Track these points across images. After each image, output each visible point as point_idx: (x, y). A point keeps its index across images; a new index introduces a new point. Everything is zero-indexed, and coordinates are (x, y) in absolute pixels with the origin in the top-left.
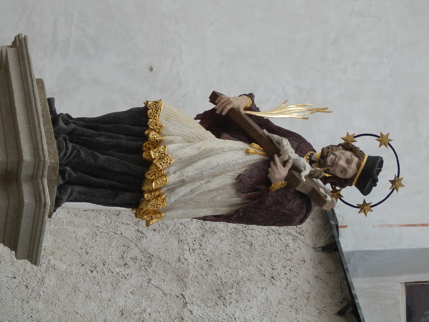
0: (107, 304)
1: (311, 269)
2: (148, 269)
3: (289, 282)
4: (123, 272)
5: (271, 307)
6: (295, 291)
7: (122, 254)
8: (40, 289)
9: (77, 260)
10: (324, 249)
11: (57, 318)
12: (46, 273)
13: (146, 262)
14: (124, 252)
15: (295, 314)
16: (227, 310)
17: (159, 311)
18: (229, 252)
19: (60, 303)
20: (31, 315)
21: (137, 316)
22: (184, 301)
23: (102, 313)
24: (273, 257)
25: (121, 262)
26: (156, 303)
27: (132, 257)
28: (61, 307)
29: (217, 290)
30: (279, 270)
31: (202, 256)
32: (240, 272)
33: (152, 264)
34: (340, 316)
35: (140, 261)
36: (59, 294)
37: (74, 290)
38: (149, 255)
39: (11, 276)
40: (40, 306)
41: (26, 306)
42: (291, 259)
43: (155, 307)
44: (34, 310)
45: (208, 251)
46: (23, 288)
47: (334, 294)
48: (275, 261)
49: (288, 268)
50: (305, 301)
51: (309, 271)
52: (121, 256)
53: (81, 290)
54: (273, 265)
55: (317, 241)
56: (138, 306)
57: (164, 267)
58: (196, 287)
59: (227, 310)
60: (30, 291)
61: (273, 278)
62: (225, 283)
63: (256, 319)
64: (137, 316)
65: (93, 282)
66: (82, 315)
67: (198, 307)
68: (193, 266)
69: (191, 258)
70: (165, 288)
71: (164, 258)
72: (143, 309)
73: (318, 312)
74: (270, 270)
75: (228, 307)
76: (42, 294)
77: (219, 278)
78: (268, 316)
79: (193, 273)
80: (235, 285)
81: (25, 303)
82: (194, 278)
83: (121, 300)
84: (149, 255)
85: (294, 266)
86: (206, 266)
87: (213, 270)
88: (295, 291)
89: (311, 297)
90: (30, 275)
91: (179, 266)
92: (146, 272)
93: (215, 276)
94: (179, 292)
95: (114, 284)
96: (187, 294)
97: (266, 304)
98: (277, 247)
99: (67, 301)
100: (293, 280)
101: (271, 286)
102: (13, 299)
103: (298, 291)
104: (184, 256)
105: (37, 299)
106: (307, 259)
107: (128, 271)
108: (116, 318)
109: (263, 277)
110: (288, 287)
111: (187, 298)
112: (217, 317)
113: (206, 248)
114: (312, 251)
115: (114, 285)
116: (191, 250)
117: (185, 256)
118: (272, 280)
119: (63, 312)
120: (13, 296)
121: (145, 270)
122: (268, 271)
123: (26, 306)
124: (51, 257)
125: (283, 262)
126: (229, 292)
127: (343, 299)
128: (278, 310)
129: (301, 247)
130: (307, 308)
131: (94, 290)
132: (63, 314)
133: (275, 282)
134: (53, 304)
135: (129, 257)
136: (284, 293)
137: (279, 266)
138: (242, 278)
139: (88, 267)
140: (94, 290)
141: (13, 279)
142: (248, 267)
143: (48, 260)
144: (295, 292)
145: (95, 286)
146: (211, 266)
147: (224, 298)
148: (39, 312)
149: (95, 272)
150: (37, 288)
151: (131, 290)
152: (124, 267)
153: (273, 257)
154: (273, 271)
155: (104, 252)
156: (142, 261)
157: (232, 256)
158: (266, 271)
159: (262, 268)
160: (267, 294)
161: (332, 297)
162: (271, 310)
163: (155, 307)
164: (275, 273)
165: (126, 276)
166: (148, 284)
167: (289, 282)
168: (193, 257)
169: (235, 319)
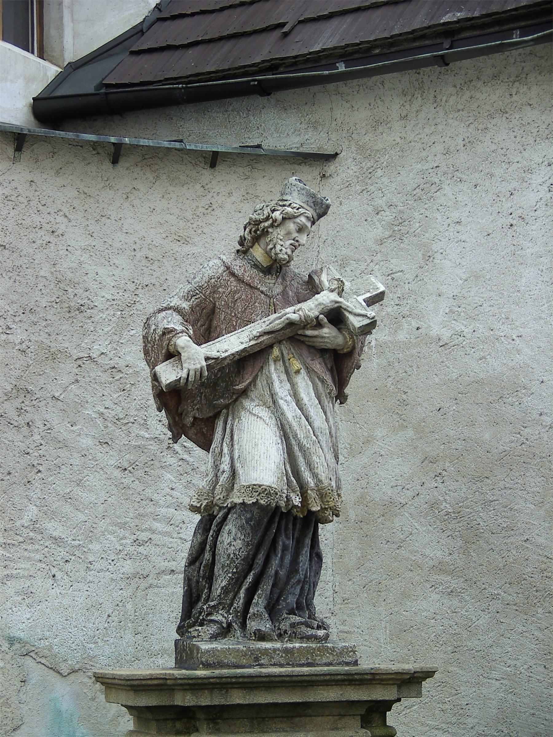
0: (90, 460)
1: (45, 176)
2: (37, 396)
3: (62, 213)
4: (41, 430)
5: (96, 247)
6: (74, 208)
7: (12, 426)
8: (70, 545)
9: (21, 488)
10: (19, 149)
11: (114, 528)
12: (44, 533)
13: (25, 396)
14: (9, 423)
15: (110, 220)
16: (100, 307)
17: (101, 395)
18: (12, 280)
19: (90, 520)
20: (110, 561)
21: (110, 425)
22: (85, 359)
23: (105, 470)
24: (24, 222)
25: (25, 430)
26: (89, 396)
27: (17, 413)
28: (96, 520)
29: (70, 311)
30: (42, 220)
31: (17, 319)
32: (42, 273)
33: (30, 390)
34: (117, 163)
35: (23, 404)
36: (77, 520)
37: (69, 500)
38: (14, 391)
39: (51, 581)
40: (95, 547)
41: (97, 566)
42: (28, 199)
43: (95, 399)
44: (103, 556)
45: (9, 309)
46: (69, 566)
47: (84, 159)
48: (28, 221)
49: (41, 207)
50: (92, 200)
51: (47, 180)
52: (15, 428)
53: (68, 491)
54: (34, 226)
55: (4, 154)
56: (94, 421)
57: (34, 374)
58: (64, 338)
59: (100, 307)
60: (73, 558)
61: (53, 232)
62: (58, 298)
63: (114, 273)
64: (110, 425)
65: (55, 472)
66: (108, 495)
67: (96, 343)
68: (32, 335)
69: (18, 336)
70: (65, 380)
71: (20, 371)
72: (98, 415)
73: (108, 189)
74: (41, 233)
75: (96, 304)
76: (77, 542)
77: (50, 304)
78: (110, 257)
79: (43, 337)
80: (62, 286)
81: (92, 567)
82: (51, 337)
83: (84, 441)
84: (14, 391)
85: (38, 197)
86: (33, 318)
87: (39, 310)
88: (74, 208)
89: (86, 191)
90: (48, 555)
91: (33, 354)
92: (41, 400)
93: (47, 309)
94: (73, 363)
95: (58, 446)
96: (76, 353)
97: (91, 254)
98: (8, 211)
99: (86, 511)
100: (59, 207)
101: (279, 232)
102: (88, 581)
103: (75, 205)
104: (17, 343)
105: (86, 550)
106: (29, 177)
107: (39, 424)
108: (111, 453)
109: (50, 245)
110: (69, 217)
111: (81, 355)
112: (111, 323)
113: (6, 310)
114: (19, 167)
115: (61, 445)
116: (8, 332)
117: (17, 342)
118: (56, 234)
119: (104, 519)
120: (83, 581)
121: (37, 400)
122: (43, 236)
123: (97, 566)
124: (18, 523)
125: (31, 212)
126: (72, 297)
127: (94, 150)
128: (101, 240)
129: (11, 179)
130: (101, 201)
131: (68, 473)
132: (108, 520)
133: (60, 232)
134: (92, 530)
135: (16, 418)
136: (77, 225)
137: (37, 219)
138: (52, 273)
139: (32, 475)
140: (68, 473)
141: (56, 578)
142: (36, 262)
143: (22, 528)
144: (76, 209)
145: (62, 471)
146: (33, 311)
147: (82, 305)
148: (105, 549)
149: (41, 468)
150: (68, 547)
151: (68, 425)
152: (31, 427)
153: (24, 222)
154: (43, 229)
155: (8, 450)
156: (23, 402)
157: (18, 278)
158: (43, 238)
159: (39, 242)
160: (76, 247)
161: (89, 164)
162: (102, 249)
163: (95, 399)
164: (46, 227)
165: (46, 428)
166: (59, 402)
167: (62, 213)
168: (19, 331)
169: (114, 300)
